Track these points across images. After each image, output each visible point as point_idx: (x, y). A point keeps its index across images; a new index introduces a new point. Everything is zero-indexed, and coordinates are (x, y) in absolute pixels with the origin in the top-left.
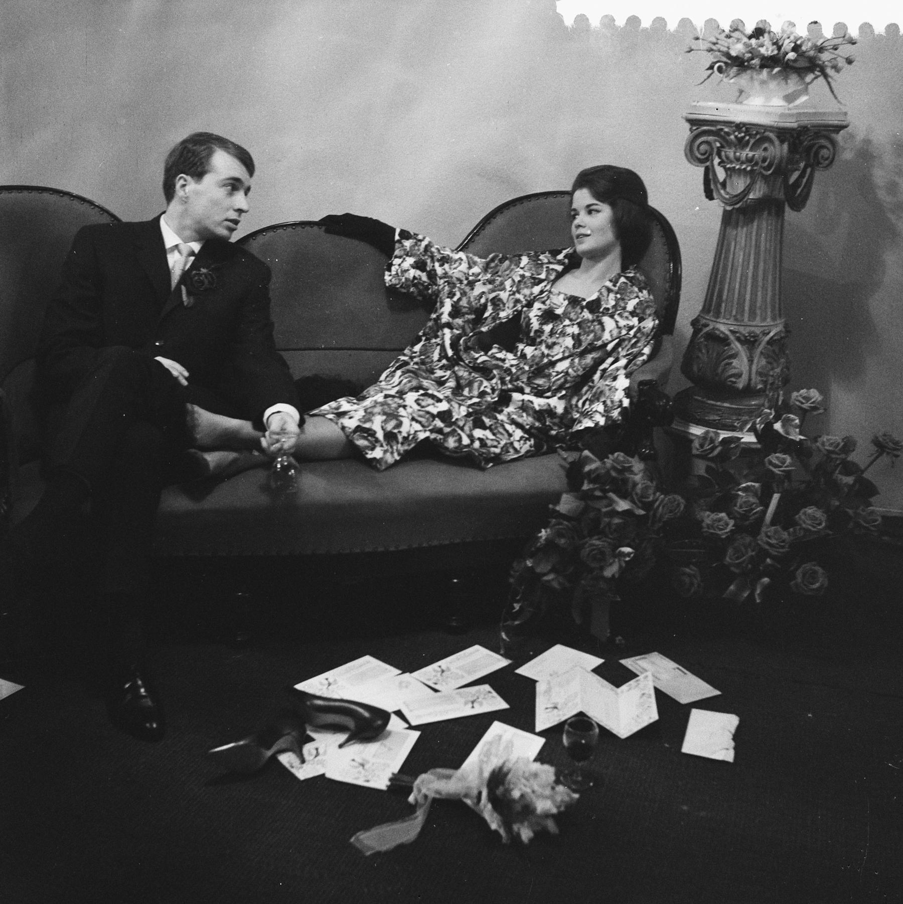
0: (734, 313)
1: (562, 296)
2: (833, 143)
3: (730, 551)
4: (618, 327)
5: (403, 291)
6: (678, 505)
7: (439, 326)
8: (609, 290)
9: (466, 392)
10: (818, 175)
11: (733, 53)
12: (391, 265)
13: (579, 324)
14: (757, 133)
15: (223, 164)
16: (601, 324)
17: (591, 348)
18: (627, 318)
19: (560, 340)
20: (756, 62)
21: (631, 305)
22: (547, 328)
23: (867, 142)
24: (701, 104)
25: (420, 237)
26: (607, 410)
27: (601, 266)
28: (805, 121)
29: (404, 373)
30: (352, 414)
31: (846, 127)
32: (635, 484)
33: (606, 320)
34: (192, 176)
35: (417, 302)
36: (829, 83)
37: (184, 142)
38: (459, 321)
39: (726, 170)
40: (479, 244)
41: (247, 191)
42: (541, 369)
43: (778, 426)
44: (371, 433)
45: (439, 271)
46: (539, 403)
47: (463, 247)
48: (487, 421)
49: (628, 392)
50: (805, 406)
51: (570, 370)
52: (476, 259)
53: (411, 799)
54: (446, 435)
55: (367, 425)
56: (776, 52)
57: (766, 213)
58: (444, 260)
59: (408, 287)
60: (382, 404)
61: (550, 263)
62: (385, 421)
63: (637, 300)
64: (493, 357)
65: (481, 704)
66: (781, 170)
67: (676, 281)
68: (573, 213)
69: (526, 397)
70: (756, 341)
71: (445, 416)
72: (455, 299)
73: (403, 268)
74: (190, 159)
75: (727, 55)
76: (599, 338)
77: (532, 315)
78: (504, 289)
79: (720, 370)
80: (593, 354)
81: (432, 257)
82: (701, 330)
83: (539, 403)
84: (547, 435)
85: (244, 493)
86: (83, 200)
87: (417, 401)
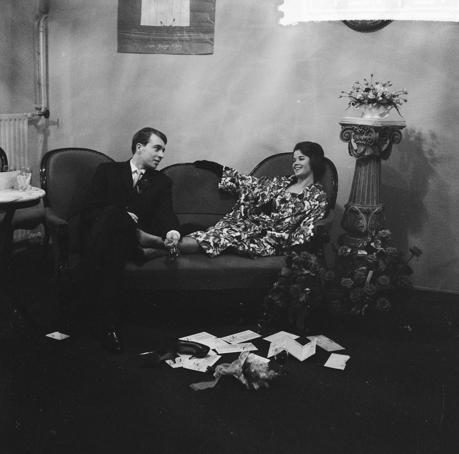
0: (360, 201)
1: (289, 193)
2: (400, 133)
3: (352, 293)
4: (310, 205)
5: (226, 190)
6: (332, 275)
7: (240, 204)
8: (307, 190)
9: (249, 230)
10: (394, 145)
11: (358, 98)
12: (221, 180)
13: (295, 204)
14: (367, 129)
15: (154, 139)
16: (304, 204)
17: (299, 213)
18: (314, 201)
19: (287, 210)
20: (366, 101)
21: (316, 197)
22: (282, 206)
23: (420, 133)
24: (346, 118)
25: (233, 170)
26: (305, 237)
27: (305, 181)
28: (387, 124)
29: (224, 222)
30: (201, 236)
31: (405, 127)
32: (311, 264)
33: (306, 202)
34: (142, 144)
35: (231, 195)
36: (397, 110)
37: (140, 131)
38: (248, 203)
39: (357, 143)
40: (258, 172)
41: (164, 150)
42: (279, 221)
43: (372, 244)
44: (209, 243)
45: (240, 183)
46: (277, 234)
47: (251, 175)
48: (256, 241)
49: (313, 230)
50: (384, 236)
51: (291, 222)
52: (256, 178)
53: (214, 374)
54: (239, 245)
55: (207, 240)
56: (375, 97)
57: (372, 162)
58: (243, 179)
59: (228, 189)
60: (213, 232)
61: (285, 180)
62: (214, 239)
63: (319, 194)
64: (261, 217)
65: (247, 348)
66: (375, 144)
67: (335, 188)
68: (294, 160)
69: (273, 232)
70: (369, 213)
71: (238, 238)
72: (246, 194)
73: (226, 181)
74: (142, 137)
75: (356, 98)
76: (303, 209)
77: (276, 200)
78: (267, 190)
79: (355, 225)
80: (301, 216)
81: (238, 177)
82: (348, 208)
83: (277, 234)
84: (280, 247)
85: (158, 265)
86: (101, 154)
87: (227, 232)
